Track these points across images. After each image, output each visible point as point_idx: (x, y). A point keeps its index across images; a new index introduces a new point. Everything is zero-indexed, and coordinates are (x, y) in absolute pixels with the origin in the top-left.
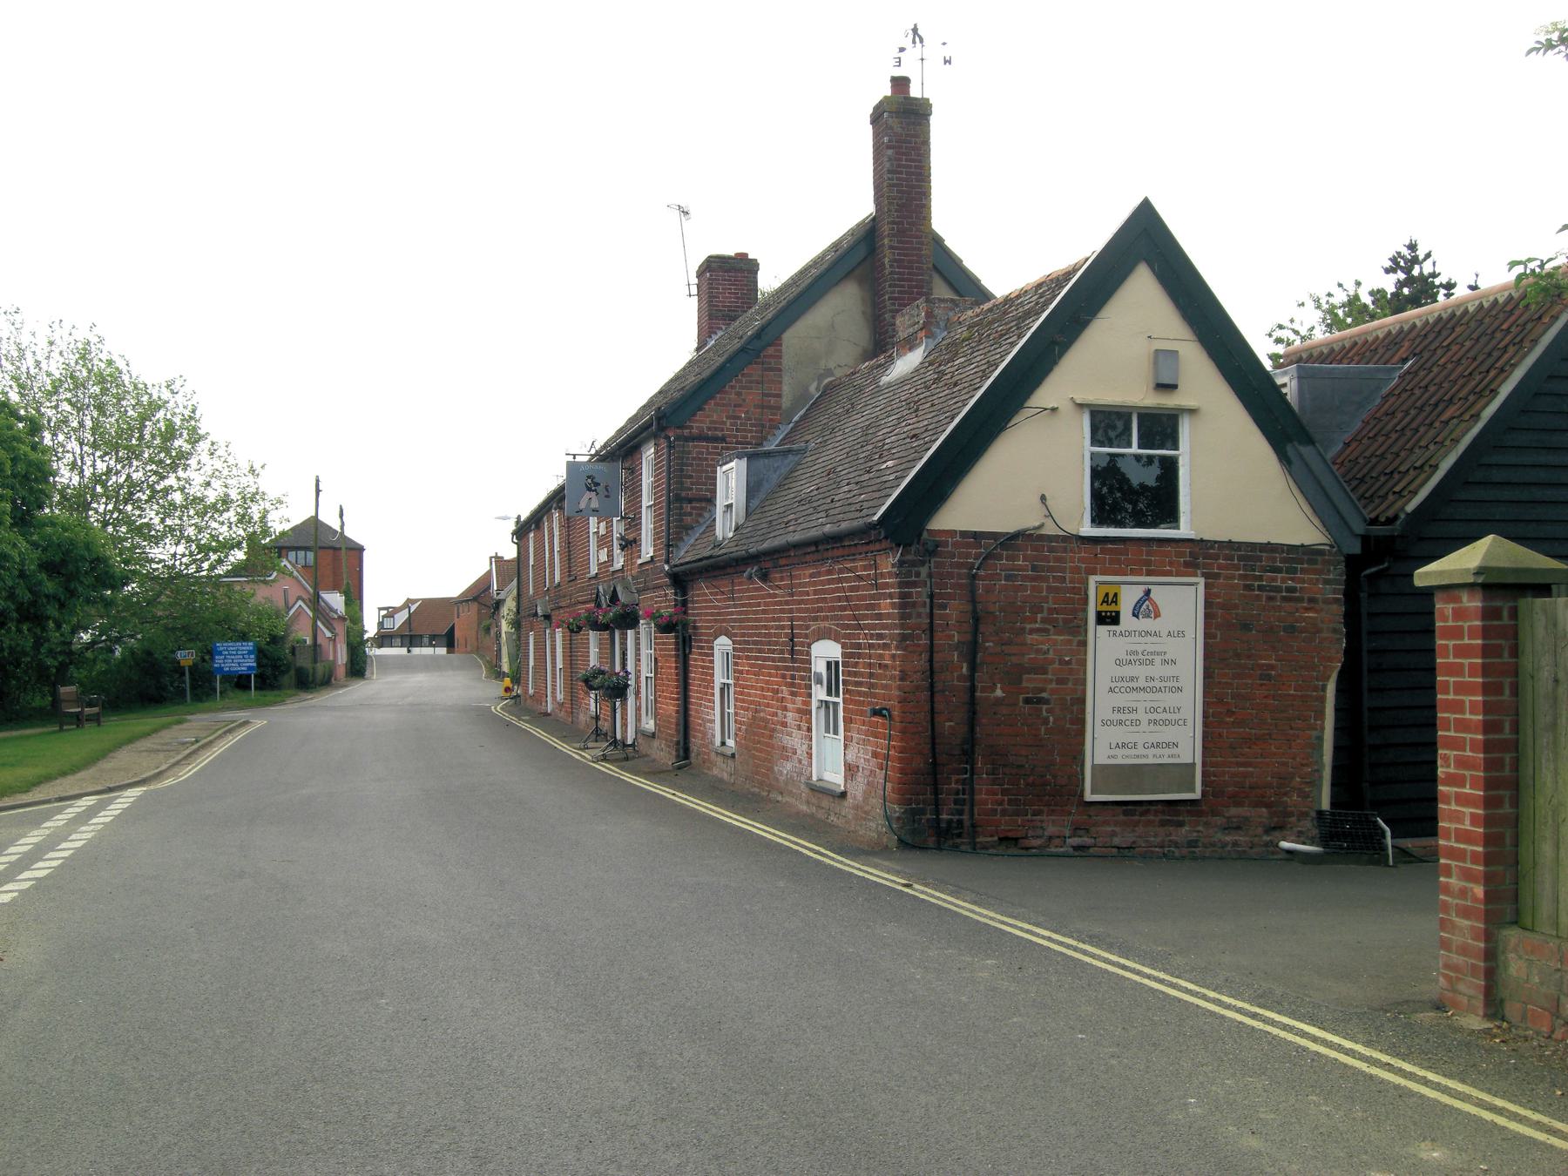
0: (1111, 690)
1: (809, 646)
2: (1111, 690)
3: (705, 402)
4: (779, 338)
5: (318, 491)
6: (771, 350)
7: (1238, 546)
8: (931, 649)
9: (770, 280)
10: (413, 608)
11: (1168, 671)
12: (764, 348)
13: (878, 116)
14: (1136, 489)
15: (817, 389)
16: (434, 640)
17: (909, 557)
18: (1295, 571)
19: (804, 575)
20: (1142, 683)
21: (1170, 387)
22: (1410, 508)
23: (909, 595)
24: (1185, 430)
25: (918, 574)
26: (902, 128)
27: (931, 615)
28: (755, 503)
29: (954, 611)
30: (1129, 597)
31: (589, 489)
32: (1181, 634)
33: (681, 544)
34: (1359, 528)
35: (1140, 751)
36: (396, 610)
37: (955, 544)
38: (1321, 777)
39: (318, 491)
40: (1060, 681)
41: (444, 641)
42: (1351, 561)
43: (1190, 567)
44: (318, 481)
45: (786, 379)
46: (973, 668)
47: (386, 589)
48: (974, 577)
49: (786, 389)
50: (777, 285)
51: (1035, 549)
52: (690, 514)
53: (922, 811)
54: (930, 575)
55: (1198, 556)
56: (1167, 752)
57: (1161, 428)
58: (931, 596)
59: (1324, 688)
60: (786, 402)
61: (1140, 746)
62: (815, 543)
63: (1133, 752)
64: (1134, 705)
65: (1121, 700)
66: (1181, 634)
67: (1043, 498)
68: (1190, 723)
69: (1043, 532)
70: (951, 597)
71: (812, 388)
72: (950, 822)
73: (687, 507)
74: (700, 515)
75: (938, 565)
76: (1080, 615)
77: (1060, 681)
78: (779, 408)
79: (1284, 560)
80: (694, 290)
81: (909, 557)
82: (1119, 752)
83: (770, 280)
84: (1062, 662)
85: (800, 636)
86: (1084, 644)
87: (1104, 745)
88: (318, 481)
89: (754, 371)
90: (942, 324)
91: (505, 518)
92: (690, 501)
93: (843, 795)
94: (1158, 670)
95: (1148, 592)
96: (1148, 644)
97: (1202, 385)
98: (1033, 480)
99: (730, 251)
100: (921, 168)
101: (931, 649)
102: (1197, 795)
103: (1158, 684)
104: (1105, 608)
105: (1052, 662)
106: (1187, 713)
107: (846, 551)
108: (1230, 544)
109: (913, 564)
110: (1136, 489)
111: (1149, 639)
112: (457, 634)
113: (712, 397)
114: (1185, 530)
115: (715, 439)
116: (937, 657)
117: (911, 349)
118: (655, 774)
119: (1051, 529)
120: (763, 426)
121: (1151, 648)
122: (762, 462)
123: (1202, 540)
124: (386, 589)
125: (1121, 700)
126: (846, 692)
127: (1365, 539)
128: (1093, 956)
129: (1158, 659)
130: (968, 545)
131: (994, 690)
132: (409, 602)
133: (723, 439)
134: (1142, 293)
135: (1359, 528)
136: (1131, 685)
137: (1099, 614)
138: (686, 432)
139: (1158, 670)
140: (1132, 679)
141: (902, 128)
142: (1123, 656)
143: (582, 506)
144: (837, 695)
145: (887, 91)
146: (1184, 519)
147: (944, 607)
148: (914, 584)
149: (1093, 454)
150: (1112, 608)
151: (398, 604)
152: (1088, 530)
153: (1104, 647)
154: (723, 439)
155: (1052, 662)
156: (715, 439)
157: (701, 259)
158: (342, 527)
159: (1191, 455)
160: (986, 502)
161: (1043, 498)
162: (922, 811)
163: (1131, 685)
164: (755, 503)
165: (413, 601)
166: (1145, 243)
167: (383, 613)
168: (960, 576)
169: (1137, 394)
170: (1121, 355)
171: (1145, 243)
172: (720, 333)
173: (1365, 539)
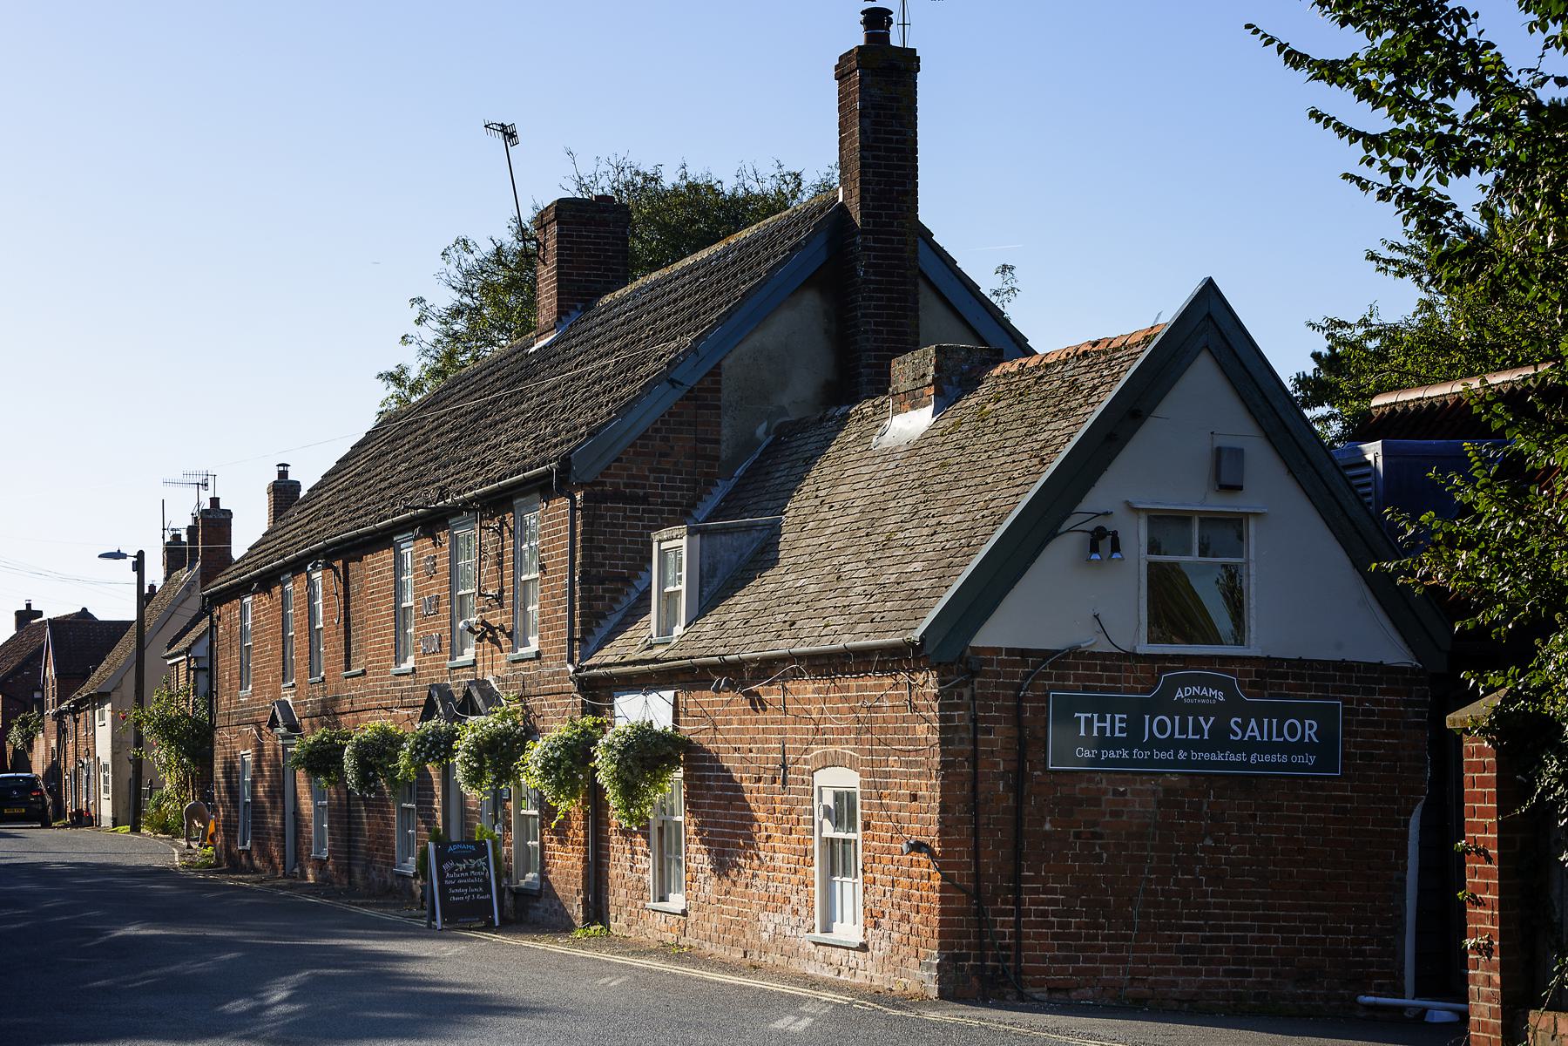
7: (1311, 663)
8: (975, 779)
15: (767, 433)
18: (1373, 691)
23: (951, 718)
25: (960, 696)
26: (880, 86)
27: (975, 742)
37: (1001, 663)
38: (1404, 924)
40: (1114, 814)
46: (1020, 800)
48: (1021, 699)
49: (726, 432)
52: (602, 598)
54: (973, 698)
58: (975, 720)
59: (1407, 824)
60: (725, 451)
67: (1096, 617)
70: (996, 720)
71: (760, 431)
72: (995, 969)
73: (599, 589)
74: (616, 600)
75: (982, 685)
76: (643, 574)
77: (1114, 814)
78: (717, 458)
84: (1116, 793)
91: (119, 555)
101: (975, 779)
105: (1105, 792)
108: (1301, 662)
116: (982, 787)
117: (913, 407)
120: (697, 482)
123: (1268, 658)
126: (867, 826)
130: (1014, 664)
131: (1042, 825)
133: (644, 500)
134: (1203, 375)
144: (852, 825)
145: (858, 38)
147: (988, 731)
148: (957, 707)
149: (1151, 565)
152: (1144, 648)
154: (644, 500)
155: (1105, 792)
159: (1261, 563)
162: (966, 958)
168: (1005, 698)
169: (1197, 497)
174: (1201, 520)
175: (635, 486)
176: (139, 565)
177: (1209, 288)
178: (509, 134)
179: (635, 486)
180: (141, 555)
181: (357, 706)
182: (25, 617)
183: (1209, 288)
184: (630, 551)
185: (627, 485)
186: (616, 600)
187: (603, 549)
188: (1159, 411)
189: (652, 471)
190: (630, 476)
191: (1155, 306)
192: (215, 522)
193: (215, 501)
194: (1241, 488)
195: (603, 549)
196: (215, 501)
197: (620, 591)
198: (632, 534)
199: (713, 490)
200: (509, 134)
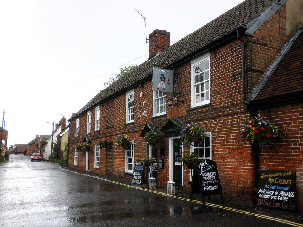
5: (4, 113)
9: (173, 41)
10: (17, 146)
16: (21, 153)
28: (292, 49)
36: (13, 146)
39: (4, 113)
41: (24, 153)
44: (4, 110)
47: (12, 142)
50: (174, 43)
80: (148, 41)
83: (173, 41)
85: (108, 154)
88: (4, 110)
99: (162, 29)
112: (27, 151)
124: (12, 142)
128: (270, 218)
132: (16, 145)
151: (14, 145)
157: (151, 31)
158: (5, 128)
164: (292, 49)
165: (17, 144)
167: (10, 147)
176: (53, 124)
179: (263, 40)
181: (111, 134)
182: (37, 136)
196: (64, 117)
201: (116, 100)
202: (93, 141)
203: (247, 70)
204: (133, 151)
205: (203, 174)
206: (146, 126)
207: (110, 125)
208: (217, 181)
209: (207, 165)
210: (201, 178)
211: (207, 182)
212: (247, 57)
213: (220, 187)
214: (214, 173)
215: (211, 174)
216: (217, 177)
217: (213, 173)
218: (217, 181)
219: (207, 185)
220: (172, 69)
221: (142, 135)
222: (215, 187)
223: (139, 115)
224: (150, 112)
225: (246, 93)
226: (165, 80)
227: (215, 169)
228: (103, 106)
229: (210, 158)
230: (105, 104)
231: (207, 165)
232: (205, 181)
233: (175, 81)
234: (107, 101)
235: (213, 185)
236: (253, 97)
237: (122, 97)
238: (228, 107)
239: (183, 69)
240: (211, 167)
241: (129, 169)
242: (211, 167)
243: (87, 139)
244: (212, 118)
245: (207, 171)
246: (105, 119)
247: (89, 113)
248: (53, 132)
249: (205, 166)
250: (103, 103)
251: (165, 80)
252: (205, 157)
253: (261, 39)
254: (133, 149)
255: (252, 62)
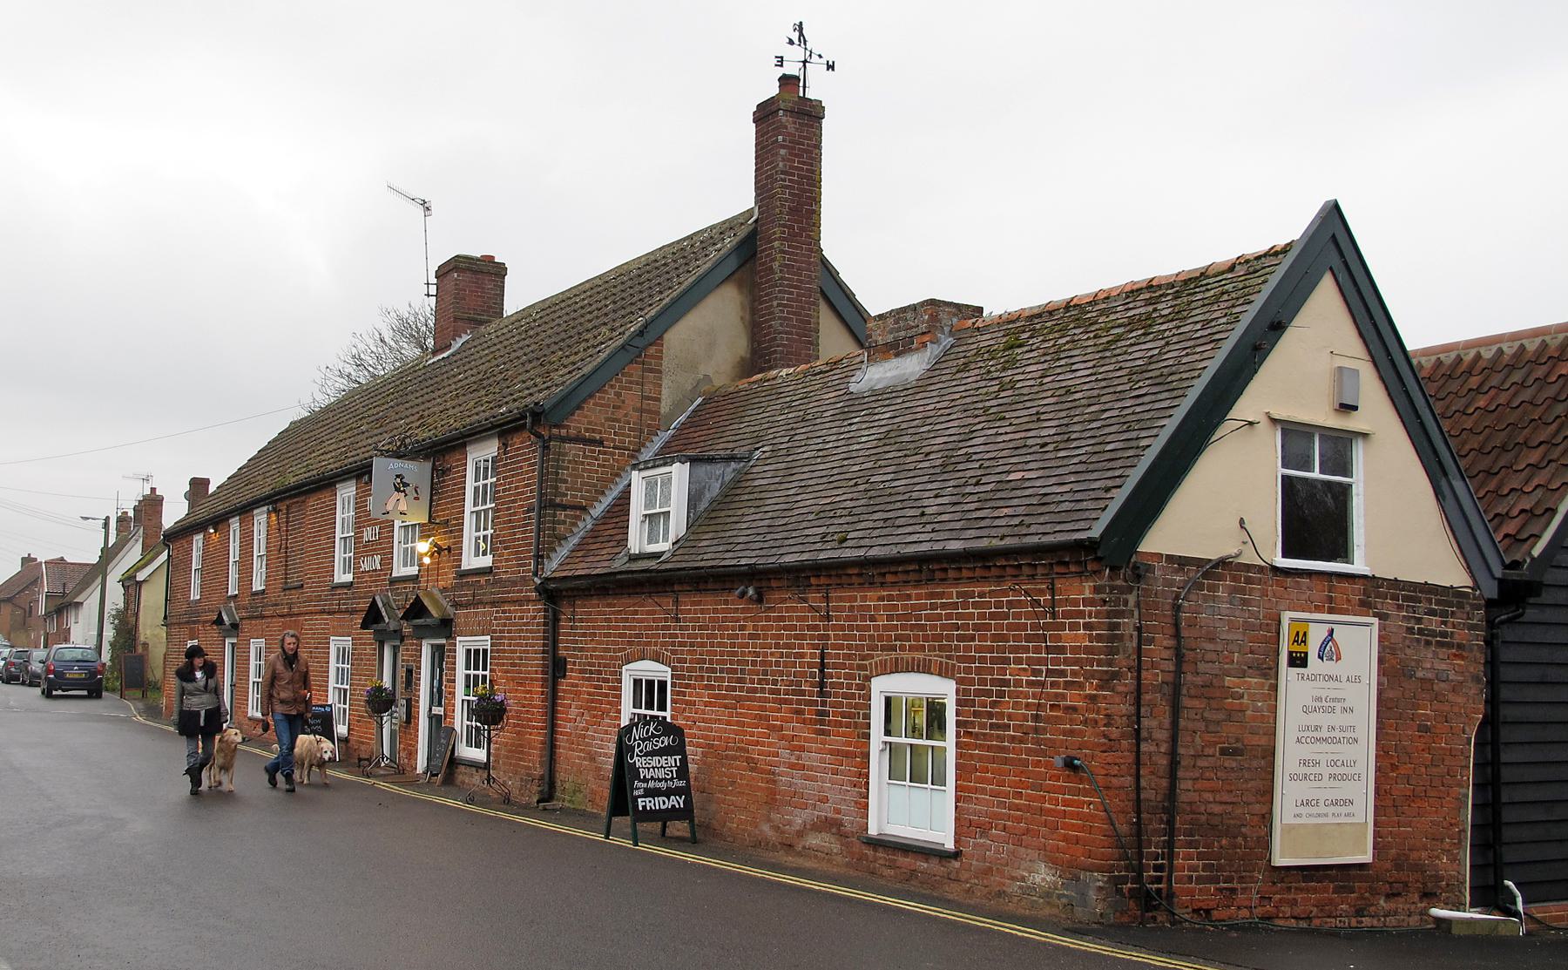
0: (1298, 741)
1: (868, 679)
2: (1298, 741)
3: (585, 401)
4: (661, 337)
6: (652, 350)
11: (1346, 720)
12: (645, 348)
13: (765, 114)
14: (1315, 520)
17: (1119, 582)
19: (870, 598)
20: (1324, 734)
21: (1347, 408)
22: (1536, 552)
23: (1116, 626)
24: (1359, 453)
25: (1126, 603)
26: (789, 129)
29: (1159, 649)
30: (1316, 635)
31: (398, 490)
32: (1358, 679)
33: (553, 555)
34: (1498, 572)
35: (1322, 809)
42: (1490, 604)
43: (1365, 606)
45: (665, 382)
49: (665, 393)
51: (1234, 579)
52: (564, 522)
53: (1124, 880)
54: (1138, 605)
55: (1372, 594)
56: (1344, 810)
57: (1339, 448)
60: (665, 407)
61: (1321, 803)
62: (922, 560)
63: (1315, 810)
64: (1317, 757)
65: (1307, 751)
66: (1358, 679)
67: (1242, 521)
68: (1287, 778)
69: (1241, 560)
73: (561, 515)
74: (575, 525)
78: (658, 413)
79: (1438, 603)
81: (1119, 582)
82: (1304, 810)
86: (1275, 688)
87: (1292, 804)
89: (635, 371)
90: (947, 329)
92: (565, 507)
93: (956, 855)
94: (1338, 719)
95: (1331, 632)
96: (1328, 690)
97: (1376, 412)
98: (1226, 506)
99: (477, 253)
100: (813, 172)
102: (1367, 858)
103: (1337, 734)
104: (1296, 648)
106: (1360, 768)
107: (901, 577)
109: (1122, 590)
110: (1315, 520)
111: (1331, 684)
113: (591, 396)
114: (1359, 565)
115: (592, 442)
118: (524, 809)
119: (1249, 558)
121: (1333, 694)
122: (703, 469)
125: (1307, 751)
127: (1501, 582)
129: (1338, 706)
133: (601, 443)
135: (1498, 572)
136: (1315, 734)
137: (1290, 653)
138: (564, 432)
139: (1338, 719)
140: (1317, 728)
141: (789, 129)
142: (1310, 703)
143: (389, 508)
146: (1358, 553)
148: (1121, 614)
150: (1302, 648)
153: (1293, 687)
154: (601, 443)
156: (592, 442)
160: (1191, 526)
161: (1242, 521)
163: (1315, 734)
166: (1331, 247)
169: (1322, 415)
170: (1311, 365)
171: (1331, 247)
172: (465, 338)
173: (1501, 582)
174: (1321, 437)
175: (594, 431)
176: (106, 525)
177: (1333, 214)
178: (426, 206)
179: (594, 431)
180: (107, 518)
181: (295, 610)
182: (27, 560)
183: (1333, 214)
184: (587, 484)
185: (587, 430)
186: (575, 525)
187: (565, 481)
188: (1297, 321)
189: (607, 419)
190: (590, 423)
191: (1288, 224)
192: (151, 505)
193: (153, 490)
194: (1355, 408)
195: (565, 481)
196: (153, 490)
197: (578, 518)
198: (590, 471)
199: (655, 439)
200: (426, 206)
201: (313, 502)
202: (246, 625)
203: (547, 504)
204: (484, 677)
205: (639, 762)
206: (374, 602)
207: (294, 580)
208: (682, 783)
209: (653, 736)
210: (635, 772)
211: (651, 784)
212: (548, 477)
213: (688, 802)
214: (673, 761)
215: (663, 762)
216: (683, 772)
217: (671, 760)
218: (682, 783)
219: (650, 793)
220: (426, 458)
221: (364, 626)
222: (676, 801)
223: (365, 567)
224: (387, 562)
225: (539, 558)
226: (408, 490)
227: (678, 749)
228: (276, 511)
229: (668, 714)
230: (282, 506)
231: (653, 736)
232: (645, 780)
233: (434, 490)
234: (290, 497)
235: (668, 793)
236: (552, 566)
237: (324, 496)
238: (514, 583)
239: (452, 460)
240: (666, 741)
241: (469, 744)
242: (666, 741)
243: (225, 618)
244: (493, 604)
245: (652, 754)
246: (281, 554)
247: (235, 524)
248: (108, 554)
249: (648, 739)
250: (275, 502)
251: (408, 490)
252: (943, 737)
253: (587, 430)
254: (485, 669)
255: (557, 488)
